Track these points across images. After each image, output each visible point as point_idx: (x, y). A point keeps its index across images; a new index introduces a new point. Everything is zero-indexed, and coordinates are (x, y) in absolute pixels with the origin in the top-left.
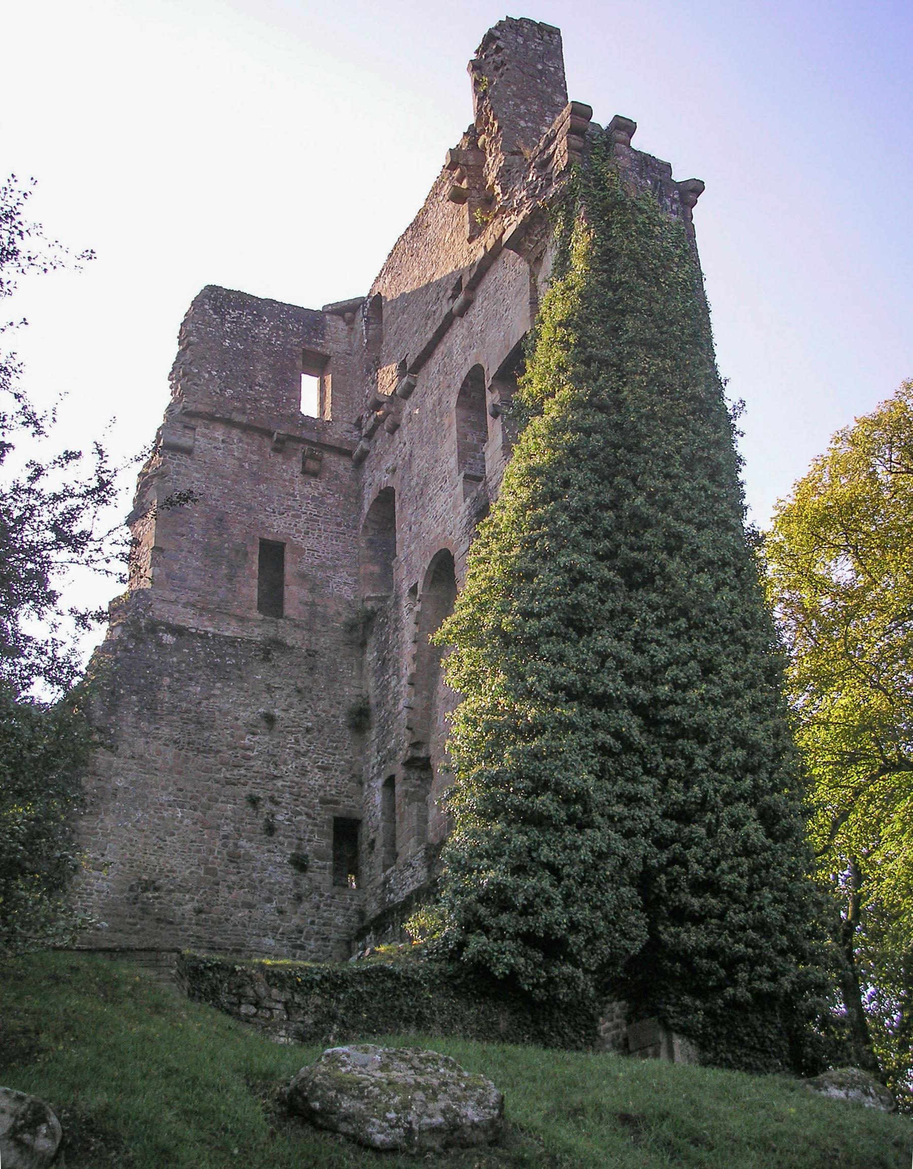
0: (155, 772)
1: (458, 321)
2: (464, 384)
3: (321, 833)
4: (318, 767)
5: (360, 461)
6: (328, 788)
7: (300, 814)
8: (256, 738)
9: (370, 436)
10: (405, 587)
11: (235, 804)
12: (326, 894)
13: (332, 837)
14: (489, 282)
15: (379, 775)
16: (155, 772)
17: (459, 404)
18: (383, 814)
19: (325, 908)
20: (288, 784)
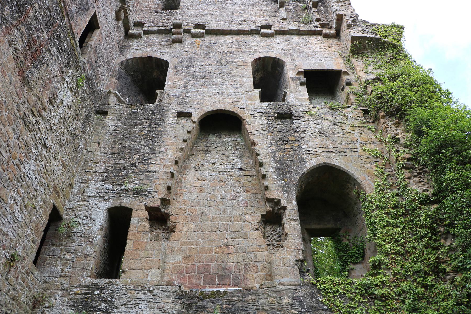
0: (343, 150)
1: (320, 37)
2: (259, 58)
3: (45, 210)
4: (62, 162)
5: (128, 36)
6: (60, 181)
7: (42, 185)
8: (51, 107)
9: (146, 33)
10: (174, 108)
11: (18, 139)
12: (27, 268)
13: (48, 219)
14: (294, 38)
15: (104, 196)
16: (343, 150)
17: (252, 62)
18: (101, 229)
19: (20, 281)
20: (47, 157)
